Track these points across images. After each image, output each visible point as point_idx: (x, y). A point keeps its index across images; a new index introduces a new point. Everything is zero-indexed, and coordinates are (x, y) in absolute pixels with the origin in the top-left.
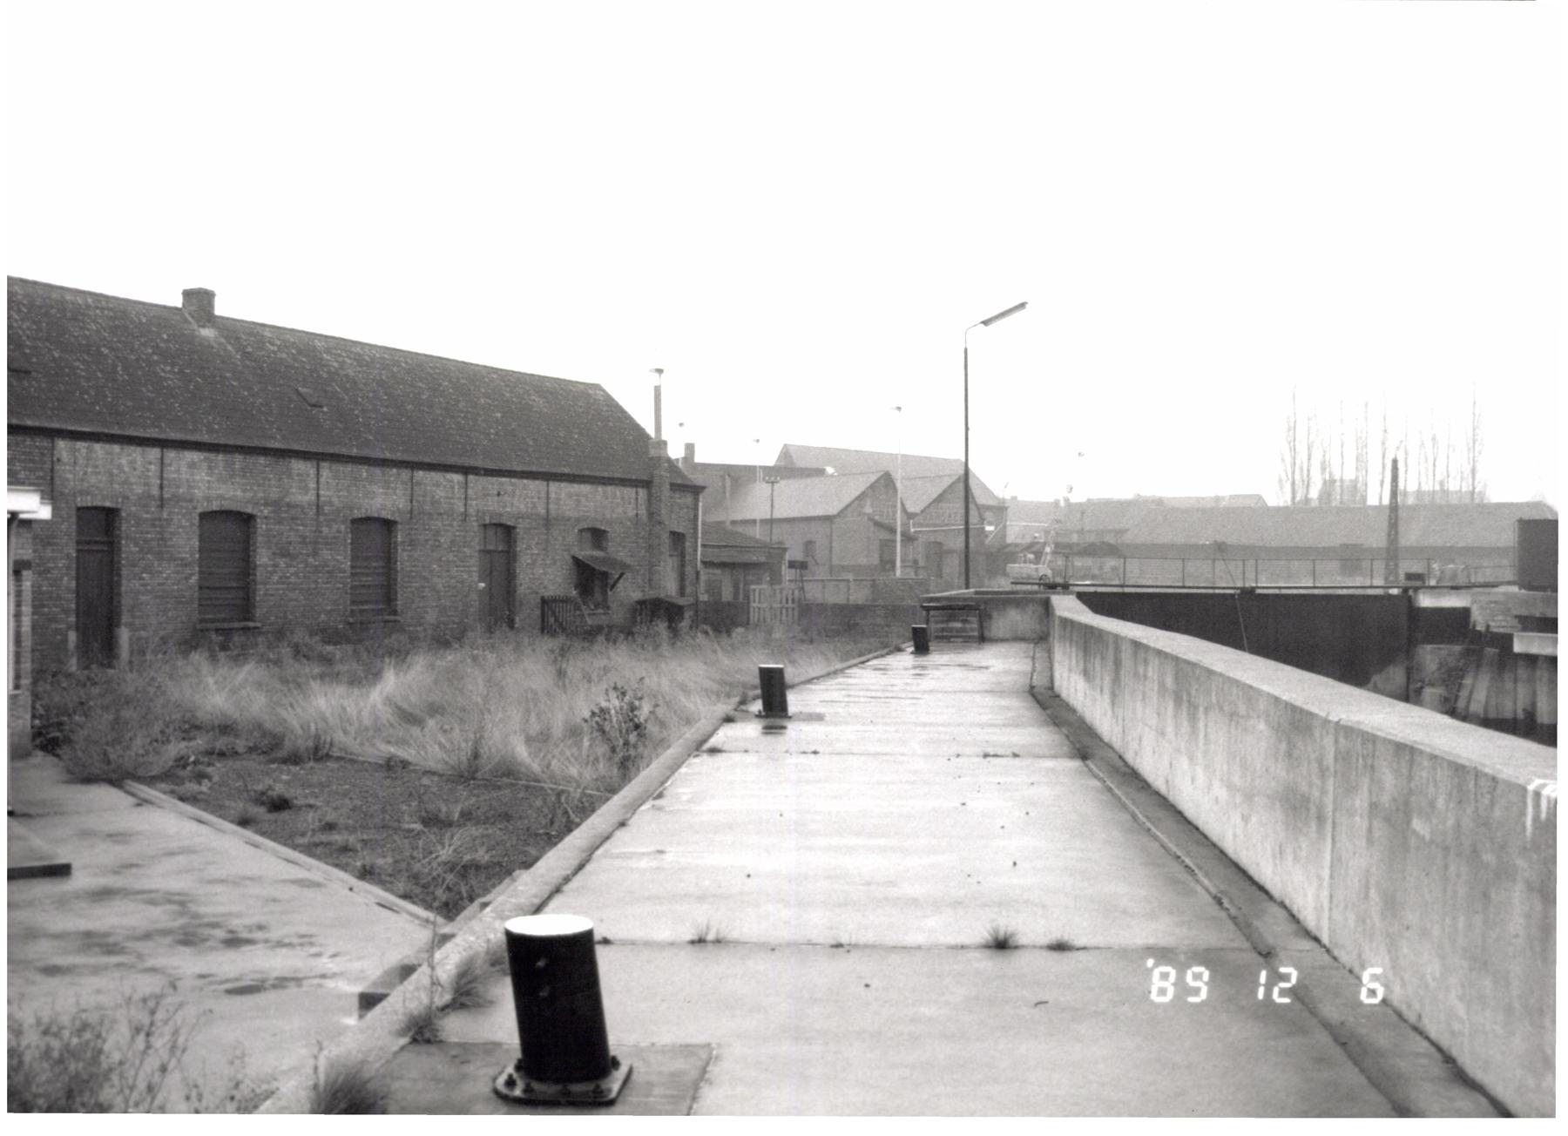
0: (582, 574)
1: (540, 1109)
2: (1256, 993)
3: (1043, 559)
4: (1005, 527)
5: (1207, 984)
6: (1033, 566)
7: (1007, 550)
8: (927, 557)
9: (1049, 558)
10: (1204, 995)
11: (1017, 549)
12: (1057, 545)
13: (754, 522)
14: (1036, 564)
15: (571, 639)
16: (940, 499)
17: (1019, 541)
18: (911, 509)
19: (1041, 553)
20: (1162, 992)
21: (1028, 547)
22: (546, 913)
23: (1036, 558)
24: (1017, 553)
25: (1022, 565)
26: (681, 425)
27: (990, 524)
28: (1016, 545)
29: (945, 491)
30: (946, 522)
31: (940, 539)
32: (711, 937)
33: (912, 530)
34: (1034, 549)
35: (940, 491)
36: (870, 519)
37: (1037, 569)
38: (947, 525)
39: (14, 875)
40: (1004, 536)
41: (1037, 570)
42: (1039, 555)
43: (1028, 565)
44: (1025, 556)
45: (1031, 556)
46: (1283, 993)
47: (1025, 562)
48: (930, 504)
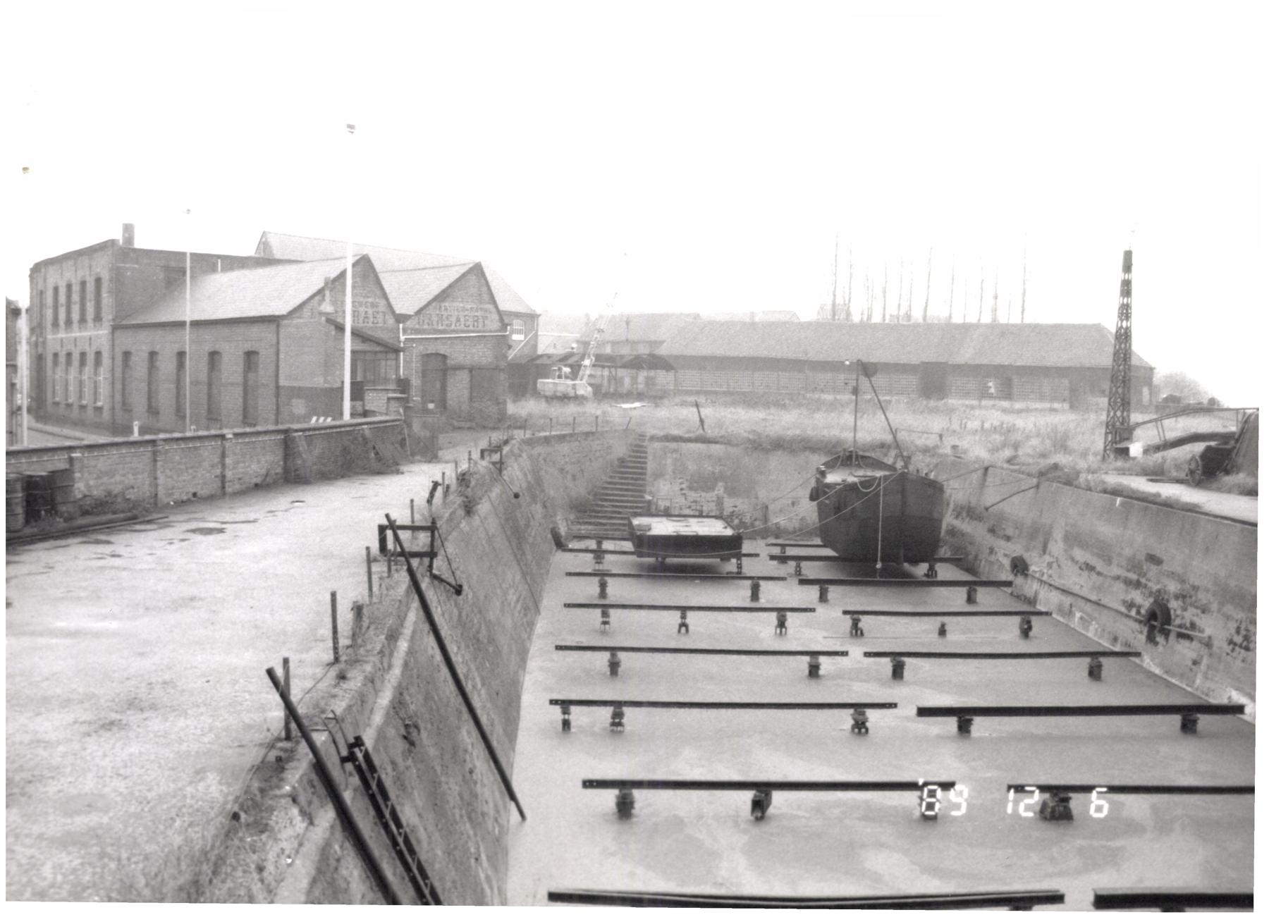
0: (846, 490)
1: (986, 906)
2: (1005, 807)
3: (581, 373)
4: (536, 336)
5: (1092, 802)
6: (570, 382)
7: (538, 362)
8: (424, 374)
9: (588, 372)
10: (963, 810)
11: (548, 362)
12: (599, 357)
13: (181, 324)
14: (573, 380)
15: (1016, 575)
16: (443, 296)
17: (551, 351)
18: (400, 309)
19: (580, 366)
20: (1099, 809)
21: (564, 359)
22: (511, 775)
23: (572, 372)
24: (551, 365)
25: (557, 381)
26: (25, 169)
27: (519, 332)
28: (549, 356)
29: (450, 286)
30: (453, 327)
31: (442, 350)
32: (120, 778)
33: (402, 338)
34: (570, 361)
35: (445, 284)
36: (329, 321)
37: (574, 385)
38: (454, 331)
39: (1251, 790)
40: (535, 346)
41: (574, 386)
42: (576, 369)
43: (562, 381)
44: (560, 369)
45: (567, 370)
46: (1028, 808)
47: (560, 377)
48: (429, 303)
